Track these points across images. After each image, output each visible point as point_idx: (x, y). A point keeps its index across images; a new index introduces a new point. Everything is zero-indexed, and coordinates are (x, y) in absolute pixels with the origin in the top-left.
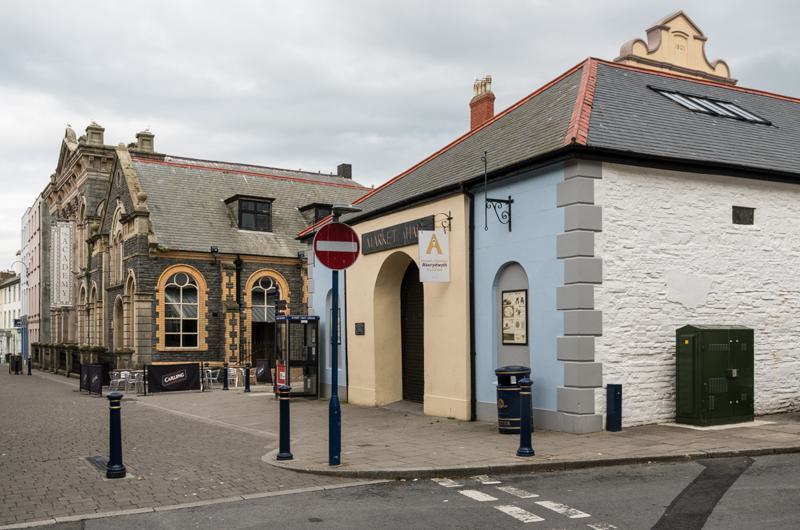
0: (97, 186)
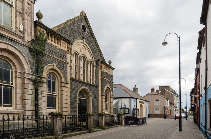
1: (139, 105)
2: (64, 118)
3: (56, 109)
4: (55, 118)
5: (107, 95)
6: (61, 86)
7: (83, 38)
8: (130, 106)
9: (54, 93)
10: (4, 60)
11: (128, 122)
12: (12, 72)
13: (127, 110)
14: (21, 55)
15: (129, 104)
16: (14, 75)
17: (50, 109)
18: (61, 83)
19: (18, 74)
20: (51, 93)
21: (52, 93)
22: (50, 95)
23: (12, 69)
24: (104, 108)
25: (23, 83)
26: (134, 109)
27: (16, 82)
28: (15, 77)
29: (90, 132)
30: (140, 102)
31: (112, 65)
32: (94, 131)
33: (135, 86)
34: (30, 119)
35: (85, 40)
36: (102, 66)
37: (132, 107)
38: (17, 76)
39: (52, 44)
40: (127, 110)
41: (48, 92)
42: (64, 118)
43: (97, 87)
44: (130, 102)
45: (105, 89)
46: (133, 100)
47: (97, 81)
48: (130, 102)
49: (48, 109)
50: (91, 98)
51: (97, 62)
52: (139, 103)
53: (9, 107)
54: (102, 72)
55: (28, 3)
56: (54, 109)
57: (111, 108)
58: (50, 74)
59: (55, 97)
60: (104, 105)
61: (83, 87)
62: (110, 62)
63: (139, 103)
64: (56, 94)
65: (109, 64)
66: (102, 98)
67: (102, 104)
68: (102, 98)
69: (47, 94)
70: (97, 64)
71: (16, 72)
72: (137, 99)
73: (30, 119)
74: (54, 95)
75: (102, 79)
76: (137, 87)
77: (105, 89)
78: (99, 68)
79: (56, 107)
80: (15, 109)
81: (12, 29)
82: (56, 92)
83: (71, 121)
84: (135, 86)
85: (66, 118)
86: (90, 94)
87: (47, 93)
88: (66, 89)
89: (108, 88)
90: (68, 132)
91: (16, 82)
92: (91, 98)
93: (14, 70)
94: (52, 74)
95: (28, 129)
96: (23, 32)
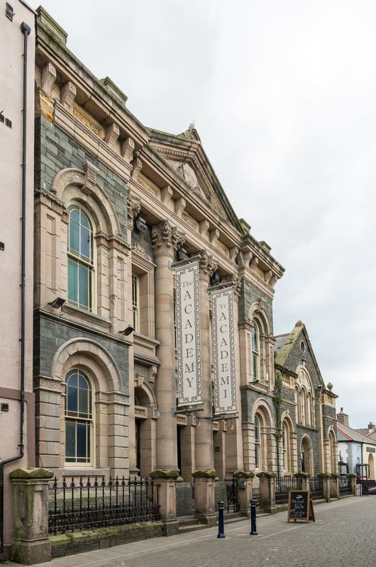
1: (366, 455)
2: (92, 485)
3: (89, 461)
4: (303, 481)
5: (256, 428)
6: (291, 438)
7: (303, 360)
8: (350, 458)
9: (86, 416)
10: (80, 371)
11: (367, 489)
12: (91, 392)
13: (344, 468)
14: (104, 355)
15: (347, 455)
16: (94, 400)
17: (73, 460)
18: (291, 433)
19: (101, 396)
20: (76, 415)
21: (81, 415)
22: (74, 420)
23: (91, 388)
24: (252, 460)
25: (269, 439)
26: (358, 466)
27: (98, 412)
28: (96, 403)
29: (327, 502)
30: (368, 450)
31: (333, 391)
32: (331, 501)
33: (342, 409)
34: (76, 486)
35: (304, 363)
36: (323, 397)
37: (355, 462)
38: (101, 401)
40: (344, 468)
41: (69, 414)
42: (92, 485)
43: (317, 431)
44: (349, 451)
45: (329, 432)
46: (355, 447)
47: (318, 423)
48: (349, 451)
49: (68, 460)
50: (312, 450)
51: (316, 391)
52: (367, 451)
53: (85, 462)
54: (323, 406)
55: (48, 215)
56: (84, 461)
57: (292, 461)
58: (76, 371)
59: (89, 426)
60: (252, 453)
61: (305, 435)
62: (330, 387)
63: (367, 451)
64: (91, 417)
65: (327, 389)
66: (325, 449)
67: (326, 459)
68: (325, 449)
69: (67, 419)
70: (317, 396)
71: (262, 428)
72: (362, 443)
73: (76, 486)
74: (84, 421)
75: (324, 418)
76: (344, 412)
77: (329, 432)
78: (320, 401)
79: (89, 456)
80: (95, 466)
81: (91, 311)
82: (91, 412)
83: (120, 493)
84: (342, 409)
85: (123, 483)
86: (311, 444)
87: (67, 416)
88: (53, 398)
89: (286, 418)
90: (55, 532)
91: (98, 412)
92: (312, 450)
93: (94, 391)
94: (81, 372)
95: (88, 509)
96: (267, 382)
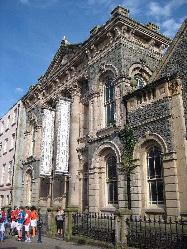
0: (127, 52)
39: (143, 106)
